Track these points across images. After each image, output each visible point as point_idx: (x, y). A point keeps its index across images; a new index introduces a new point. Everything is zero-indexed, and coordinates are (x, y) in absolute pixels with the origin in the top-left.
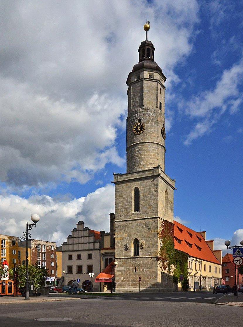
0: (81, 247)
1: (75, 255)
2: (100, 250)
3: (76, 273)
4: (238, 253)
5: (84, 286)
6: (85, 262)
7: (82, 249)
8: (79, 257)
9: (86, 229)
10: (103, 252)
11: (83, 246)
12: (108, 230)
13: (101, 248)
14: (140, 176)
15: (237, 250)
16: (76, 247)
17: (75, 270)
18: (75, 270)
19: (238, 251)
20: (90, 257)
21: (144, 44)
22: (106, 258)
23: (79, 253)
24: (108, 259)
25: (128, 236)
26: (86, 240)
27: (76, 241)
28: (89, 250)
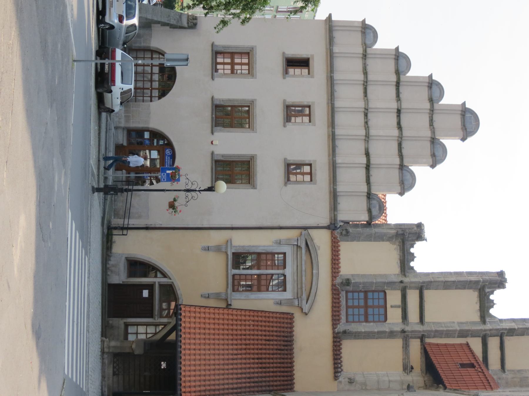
0: (349, 123)
2: (332, 227)
3: (216, 97)
5: (147, 135)
6: (267, 143)
9: (439, 153)
10: (322, 240)
11: (384, 83)
12: (426, 260)
13: (339, 230)
16: (349, 97)
23: (320, 113)
27: (383, 97)
28: (333, 167)
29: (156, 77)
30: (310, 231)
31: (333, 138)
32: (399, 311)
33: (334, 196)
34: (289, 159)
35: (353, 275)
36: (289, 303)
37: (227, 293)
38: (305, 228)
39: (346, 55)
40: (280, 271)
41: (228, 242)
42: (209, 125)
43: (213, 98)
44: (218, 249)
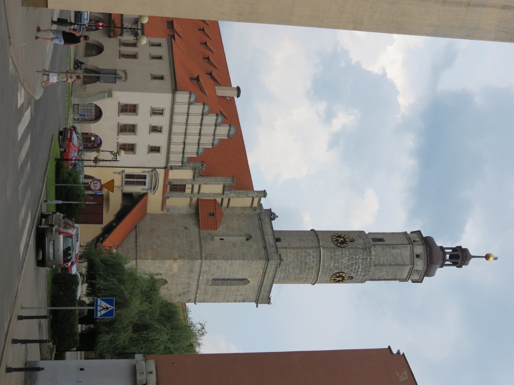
1: (162, 121)
4: (104, 309)
6: (142, 139)
7: (172, 150)
8: (155, 129)
10: (161, 173)
14: (266, 287)
15: (108, 306)
17: (127, 119)
18: (127, 119)
19: (107, 308)
20: (155, 149)
21: (465, 252)
23: (166, 130)
25: (173, 276)
26: (192, 139)
29: (94, 111)
31: (170, 139)
33: (168, 158)
36: (146, 189)
37: (122, 186)
38: (155, 168)
40: (144, 180)
41: (123, 171)
44: (119, 173)
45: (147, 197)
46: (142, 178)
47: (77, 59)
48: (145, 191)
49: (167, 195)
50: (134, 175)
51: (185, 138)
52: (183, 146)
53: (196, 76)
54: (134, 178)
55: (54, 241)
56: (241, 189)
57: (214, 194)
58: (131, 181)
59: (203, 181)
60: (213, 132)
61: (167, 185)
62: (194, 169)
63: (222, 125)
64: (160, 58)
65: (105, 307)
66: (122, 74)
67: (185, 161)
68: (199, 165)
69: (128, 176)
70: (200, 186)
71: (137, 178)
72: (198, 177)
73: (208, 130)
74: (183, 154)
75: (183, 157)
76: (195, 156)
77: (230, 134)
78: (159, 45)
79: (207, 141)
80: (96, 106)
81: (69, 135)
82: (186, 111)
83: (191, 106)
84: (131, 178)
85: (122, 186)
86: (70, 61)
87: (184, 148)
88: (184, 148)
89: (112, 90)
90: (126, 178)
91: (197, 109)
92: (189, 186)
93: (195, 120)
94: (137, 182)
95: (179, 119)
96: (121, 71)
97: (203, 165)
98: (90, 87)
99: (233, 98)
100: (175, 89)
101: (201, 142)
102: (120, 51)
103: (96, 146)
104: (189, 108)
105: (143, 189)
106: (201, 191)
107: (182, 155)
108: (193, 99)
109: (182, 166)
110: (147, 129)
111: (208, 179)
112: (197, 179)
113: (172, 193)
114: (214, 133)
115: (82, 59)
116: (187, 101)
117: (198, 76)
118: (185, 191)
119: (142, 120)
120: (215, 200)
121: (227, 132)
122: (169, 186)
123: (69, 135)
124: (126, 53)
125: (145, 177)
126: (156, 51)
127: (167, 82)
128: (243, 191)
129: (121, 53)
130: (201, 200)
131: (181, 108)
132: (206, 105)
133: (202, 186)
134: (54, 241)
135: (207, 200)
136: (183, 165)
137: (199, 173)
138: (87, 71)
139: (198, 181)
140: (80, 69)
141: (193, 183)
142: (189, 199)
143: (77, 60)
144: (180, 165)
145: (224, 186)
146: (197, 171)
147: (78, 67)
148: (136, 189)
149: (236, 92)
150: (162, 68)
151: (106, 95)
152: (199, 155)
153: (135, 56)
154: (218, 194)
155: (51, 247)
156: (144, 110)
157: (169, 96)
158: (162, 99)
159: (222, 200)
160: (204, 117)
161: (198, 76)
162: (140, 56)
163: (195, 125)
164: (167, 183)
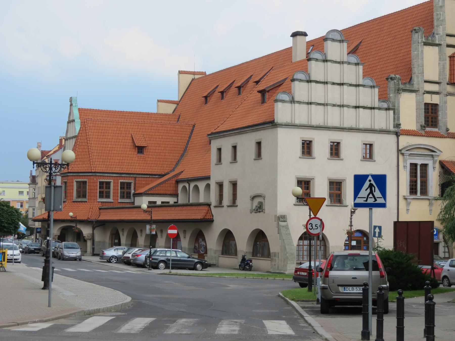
1: (321, 142)
4: (371, 192)
7: (368, 126)
8: (335, 150)
10: (405, 141)
15: (367, 184)
19: (371, 186)
22: (414, 161)
23: (336, 136)
24: (416, 165)
26: (349, 95)
30: (400, 148)
31: (350, 129)
32: (434, 96)
33: (382, 131)
34: (360, 158)
35: (417, 122)
36: (434, 163)
37: (429, 199)
38: (399, 151)
39: (326, 118)
42: (342, 208)
43: (294, 205)
44: (408, 204)
45: (447, 162)
46: (416, 169)
47: (238, 267)
48: (437, 165)
49: (443, 132)
50: (411, 181)
51: (348, 106)
52: (361, 110)
53: (259, 95)
54: (416, 182)
55: (339, 285)
56: (433, 18)
57: (440, 59)
58: (421, 186)
59: (418, 78)
60: (338, 65)
61: (426, 132)
62: (398, 91)
63: (325, 52)
64: (235, 148)
65: (369, 191)
66: (256, 202)
67: (385, 105)
68: (392, 84)
69: (413, 190)
70: (426, 82)
71: (416, 177)
72: (413, 84)
73: (333, 72)
74: (374, 108)
75: (379, 109)
76: (377, 90)
77: (339, 38)
78: (220, 150)
79: (353, 73)
80: (301, 238)
81: (303, 273)
82: (305, 106)
83: (296, 99)
84: (416, 185)
85: (429, 199)
86: (216, 274)
87: (364, 108)
88: (364, 108)
89: (275, 216)
90: (416, 193)
91: (300, 90)
92: (428, 99)
93: (318, 93)
94: (421, 177)
95: (317, 116)
96: (252, 204)
97: (391, 79)
98: (274, 247)
99: (308, 43)
100: (271, 124)
101: (354, 83)
102: (228, 206)
103: (365, 239)
104: (299, 102)
105: (434, 168)
106: (436, 79)
107: (376, 111)
108: (285, 97)
109: (394, 110)
110: (335, 163)
111: (415, 70)
112: (415, 87)
113: (441, 124)
114: (339, 63)
115: (236, 261)
116: (289, 105)
117: (259, 92)
118: (436, 105)
119: (322, 172)
120: (450, 57)
121: (337, 44)
122: (428, 129)
123: (303, 273)
124: (231, 198)
125: (414, 166)
126: (227, 155)
127: (263, 135)
128: (435, 14)
129: (231, 204)
130: (450, 79)
131: (301, 114)
132: (295, 77)
133: (426, 78)
134: (339, 285)
135: (450, 70)
136: (394, 109)
137: (405, 84)
138: (255, 253)
139: (418, 84)
140: (251, 261)
141: (422, 91)
142: (449, 97)
143: (240, 266)
144: (391, 112)
145: (426, 44)
146: (401, 86)
147: (248, 264)
148: (434, 178)
149: (298, 37)
150: (246, 143)
151: (282, 224)
152: (375, 84)
153: (234, 185)
154: (441, 53)
155: (349, 290)
156: (306, 168)
157: (281, 132)
158: (287, 143)
159: (449, 46)
160: (313, 78)
161: (259, 92)
162: (233, 178)
163: (326, 92)
164: (423, 133)
